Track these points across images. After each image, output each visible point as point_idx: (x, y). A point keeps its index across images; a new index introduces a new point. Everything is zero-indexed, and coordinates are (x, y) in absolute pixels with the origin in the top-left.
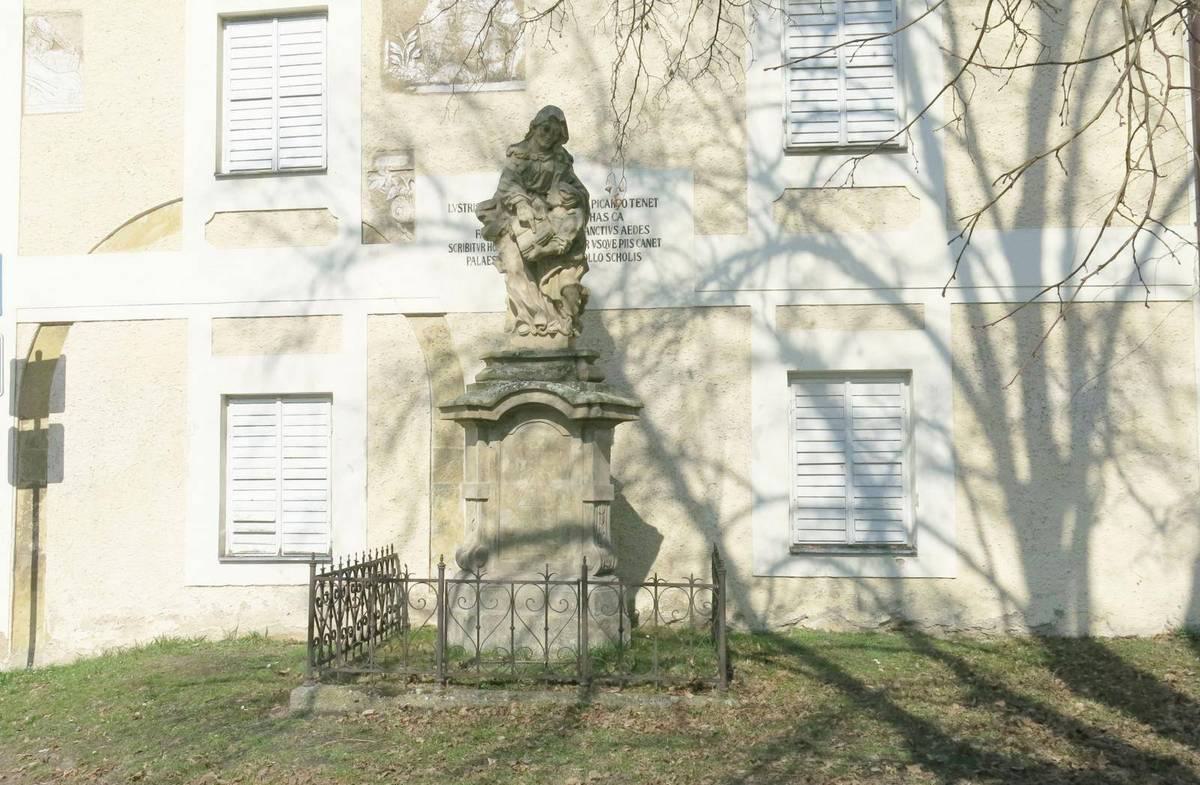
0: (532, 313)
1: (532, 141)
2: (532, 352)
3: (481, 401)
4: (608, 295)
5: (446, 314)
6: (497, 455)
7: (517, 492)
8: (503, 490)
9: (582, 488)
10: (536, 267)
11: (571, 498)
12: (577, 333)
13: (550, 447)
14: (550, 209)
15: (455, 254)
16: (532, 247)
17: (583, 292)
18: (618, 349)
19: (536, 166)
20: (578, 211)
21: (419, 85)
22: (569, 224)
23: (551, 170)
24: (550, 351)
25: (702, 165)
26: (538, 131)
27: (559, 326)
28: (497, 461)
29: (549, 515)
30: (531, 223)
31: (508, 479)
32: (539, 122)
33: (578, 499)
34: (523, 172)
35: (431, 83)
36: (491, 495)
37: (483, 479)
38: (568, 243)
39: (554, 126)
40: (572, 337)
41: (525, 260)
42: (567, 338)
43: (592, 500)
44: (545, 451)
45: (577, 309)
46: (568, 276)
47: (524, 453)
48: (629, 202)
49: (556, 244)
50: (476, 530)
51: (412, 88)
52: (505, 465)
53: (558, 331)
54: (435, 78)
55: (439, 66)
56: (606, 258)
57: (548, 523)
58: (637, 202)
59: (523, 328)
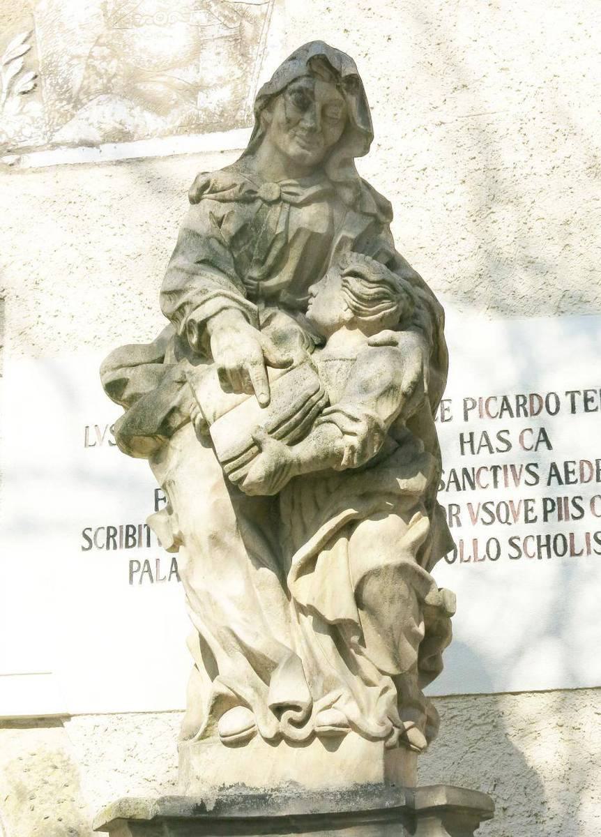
0: (263, 667)
1: (265, 151)
2: (262, 799)
4: (519, 653)
5: (68, 717)
10: (274, 515)
12: (417, 737)
14: (319, 338)
15: (100, 555)
16: (257, 444)
17: (431, 598)
18: (555, 806)
19: (275, 219)
20: (406, 338)
21: (28, 150)
22: (378, 369)
23: (322, 228)
24: (323, 795)
26: (280, 113)
27: (347, 710)
30: (256, 373)
32: (279, 86)
34: (235, 239)
35: (55, 146)
38: (375, 428)
39: (324, 91)
40: (398, 747)
41: (234, 488)
42: (379, 746)
45: (411, 653)
46: (382, 540)
48: (566, 402)
49: (331, 430)
51: (10, 159)
53: (351, 725)
54: (69, 133)
55: (77, 103)
56: (507, 549)
58: (586, 400)
59: (233, 721)
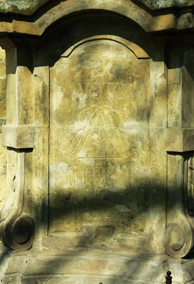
3: (15, 7)
6: (44, 87)
7: (75, 141)
8: (53, 134)
9: (165, 135)
11: (151, 147)
13: (120, 75)
25: (73, 193)
28: (46, 95)
29: (119, 171)
31: (61, 121)
33: (161, 148)
36: (38, 144)
37: (25, 120)
43: (181, 151)
44: (113, 80)
47: (83, 83)
50: (17, 192)
52: (57, 100)
57: (119, 181)
